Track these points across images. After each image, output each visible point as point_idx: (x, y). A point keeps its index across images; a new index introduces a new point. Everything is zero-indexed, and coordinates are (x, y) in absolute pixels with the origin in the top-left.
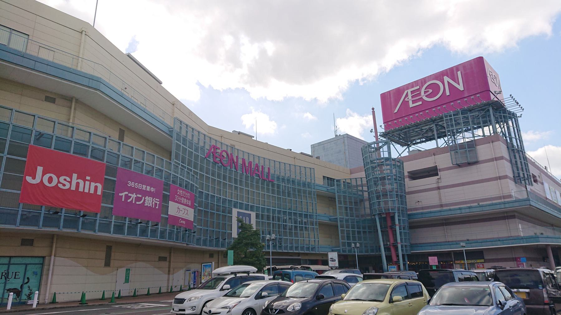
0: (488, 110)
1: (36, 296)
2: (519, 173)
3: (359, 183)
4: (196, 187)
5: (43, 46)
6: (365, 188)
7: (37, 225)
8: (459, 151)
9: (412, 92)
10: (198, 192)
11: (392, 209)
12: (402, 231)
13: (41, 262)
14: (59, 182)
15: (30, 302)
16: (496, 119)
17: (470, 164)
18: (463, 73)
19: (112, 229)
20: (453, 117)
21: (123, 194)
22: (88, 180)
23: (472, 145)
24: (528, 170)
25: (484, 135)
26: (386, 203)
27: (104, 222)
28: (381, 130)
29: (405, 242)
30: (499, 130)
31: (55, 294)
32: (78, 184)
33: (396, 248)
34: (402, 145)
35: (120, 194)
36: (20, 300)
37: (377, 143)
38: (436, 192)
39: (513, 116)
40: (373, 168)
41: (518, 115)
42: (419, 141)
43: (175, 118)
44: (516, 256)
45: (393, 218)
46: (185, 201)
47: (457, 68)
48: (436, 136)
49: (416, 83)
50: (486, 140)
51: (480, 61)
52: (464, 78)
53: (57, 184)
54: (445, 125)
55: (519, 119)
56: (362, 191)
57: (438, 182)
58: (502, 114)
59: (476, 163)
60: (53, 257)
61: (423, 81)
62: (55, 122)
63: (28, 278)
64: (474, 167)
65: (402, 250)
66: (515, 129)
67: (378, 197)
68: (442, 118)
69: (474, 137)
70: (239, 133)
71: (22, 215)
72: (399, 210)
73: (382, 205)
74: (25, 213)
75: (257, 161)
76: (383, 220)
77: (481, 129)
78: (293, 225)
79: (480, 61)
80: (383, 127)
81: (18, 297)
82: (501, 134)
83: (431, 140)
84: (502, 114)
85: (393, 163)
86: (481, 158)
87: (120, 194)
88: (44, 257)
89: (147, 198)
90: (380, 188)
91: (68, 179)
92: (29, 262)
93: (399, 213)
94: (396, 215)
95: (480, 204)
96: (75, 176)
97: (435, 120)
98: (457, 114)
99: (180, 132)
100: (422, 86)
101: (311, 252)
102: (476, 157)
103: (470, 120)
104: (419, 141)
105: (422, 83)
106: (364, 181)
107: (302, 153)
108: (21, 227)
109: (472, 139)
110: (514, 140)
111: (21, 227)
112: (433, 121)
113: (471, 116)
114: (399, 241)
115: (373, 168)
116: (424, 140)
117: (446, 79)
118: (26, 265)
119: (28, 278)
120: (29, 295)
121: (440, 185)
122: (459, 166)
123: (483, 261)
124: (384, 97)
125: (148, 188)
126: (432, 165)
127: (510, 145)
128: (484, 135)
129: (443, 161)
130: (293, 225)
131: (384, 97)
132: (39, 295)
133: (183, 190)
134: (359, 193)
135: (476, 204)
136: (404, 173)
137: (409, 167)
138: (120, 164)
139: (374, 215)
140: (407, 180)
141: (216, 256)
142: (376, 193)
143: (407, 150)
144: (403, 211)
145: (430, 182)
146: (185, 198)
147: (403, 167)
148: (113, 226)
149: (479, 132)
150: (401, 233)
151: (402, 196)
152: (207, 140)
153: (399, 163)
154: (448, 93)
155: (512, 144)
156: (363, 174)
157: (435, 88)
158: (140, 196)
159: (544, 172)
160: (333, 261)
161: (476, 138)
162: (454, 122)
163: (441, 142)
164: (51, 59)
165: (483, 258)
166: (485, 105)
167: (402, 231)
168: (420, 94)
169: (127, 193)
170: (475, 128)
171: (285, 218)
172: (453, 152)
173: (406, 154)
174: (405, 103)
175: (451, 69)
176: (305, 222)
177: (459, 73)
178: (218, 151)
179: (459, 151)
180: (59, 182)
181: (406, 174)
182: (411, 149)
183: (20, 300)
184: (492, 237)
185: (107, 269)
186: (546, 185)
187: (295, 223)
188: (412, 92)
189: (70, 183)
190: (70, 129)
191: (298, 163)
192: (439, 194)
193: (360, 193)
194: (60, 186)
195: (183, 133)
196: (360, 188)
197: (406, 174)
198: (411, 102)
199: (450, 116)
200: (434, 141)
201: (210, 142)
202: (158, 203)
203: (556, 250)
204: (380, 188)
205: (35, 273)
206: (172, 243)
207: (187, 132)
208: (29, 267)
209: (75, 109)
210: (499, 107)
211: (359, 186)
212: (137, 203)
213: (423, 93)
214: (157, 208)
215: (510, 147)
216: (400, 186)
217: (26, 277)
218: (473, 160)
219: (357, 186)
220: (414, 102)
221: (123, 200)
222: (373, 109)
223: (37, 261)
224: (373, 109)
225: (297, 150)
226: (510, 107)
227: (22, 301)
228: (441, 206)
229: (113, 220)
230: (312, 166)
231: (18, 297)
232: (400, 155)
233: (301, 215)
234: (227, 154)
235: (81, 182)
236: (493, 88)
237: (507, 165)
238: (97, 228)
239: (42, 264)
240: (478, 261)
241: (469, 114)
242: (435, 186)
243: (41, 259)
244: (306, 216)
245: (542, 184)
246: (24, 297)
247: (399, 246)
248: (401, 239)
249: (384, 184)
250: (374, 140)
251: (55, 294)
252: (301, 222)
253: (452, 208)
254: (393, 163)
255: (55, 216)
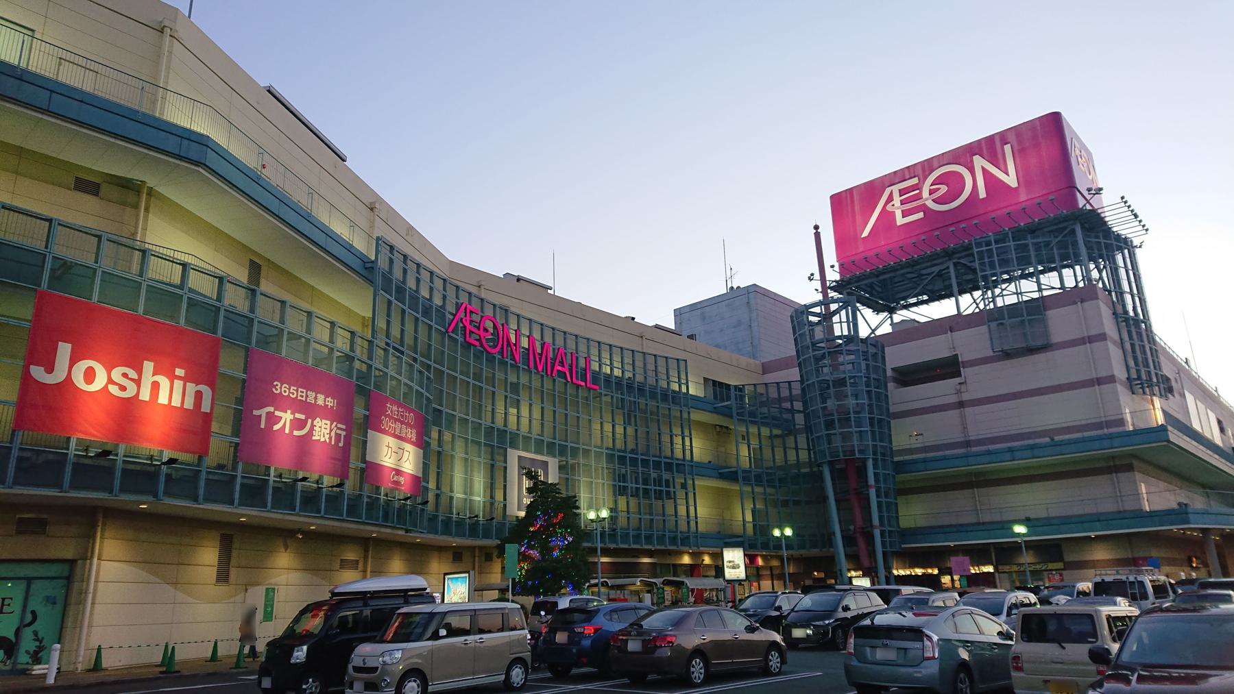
0: (1073, 232)
1: (55, 656)
2: (1138, 371)
3: (785, 393)
4: (428, 399)
5: (68, 56)
6: (798, 405)
7: (58, 485)
8: (1007, 321)
9: (902, 192)
10: (431, 411)
11: (860, 452)
12: (883, 499)
13: (66, 574)
14: (110, 381)
15: (38, 670)
16: (1089, 248)
17: (1031, 351)
18: (1016, 147)
19: (237, 495)
20: (994, 246)
21: (263, 412)
22: (179, 378)
23: (1037, 308)
24: (1157, 366)
25: (1063, 287)
26: (846, 437)
27: (216, 478)
28: (833, 275)
29: (890, 525)
30: (1095, 274)
31: (99, 649)
32: (155, 386)
33: (869, 538)
34: (877, 310)
35: (256, 412)
36: (14, 663)
37: (826, 302)
38: (955, 413)
39: (1124, 244)
40: (818, 359)
41: (1136, 242)
42: (914, 300)
43: (378, 239)
44: (1136, 555)
45: (861, 471)
46: (404, 431)
47: (1003, 137)
48: (955, 289)
49: (910, 172)
50: (1067, 297)
51: (1054, 122)
52: (1021, 174)
53: (106, 386)
54: (977, 265)
55: (1137, 251)
56: (792, 411)
57: (959, 392)
58: (1102, 241)
59: (1046, 347)
60: (95, 560)
61: (927, 166)
62: (100, 237)
63: (33, 612)
64: (1039, 358)
65: (883, 543)
66: (1131, 273)
67: (830, 425)
68: (968, 248)
69: (1040, 290)
70: (519, 279)
71: (20, 459)
72: (875, 453)
73: (837, 442)
74: (27, 454)
75: (560, 342)
76: (838, 475)
77: (1055, 274)
78: (641, 486)
79: (1054, 122)
80: (837, 268)
81: (9, 657)
82: (1100, 285)
83: (940, 298)
84: (1102, 241)
85: (862, 347)
86: (1056, 338)
87: (256, 412)
88: (72, 562)
89: (318, 422)
90: (831, 404)
91: (133, 374)
92: (35, 574)
93: (875, 460)
94: (870, 463)
95: (1056, 438)
96: (148, 366)
97: (954, 253)
98: (1003, 240)
99: (390, 272)
100: (925, 178)
101: (646, 547)
102: (1046, 333)
103: (1032, 253)
104: (914, 300)
105: (924, 171)
106: (797, 390)
107: (657, 327)
108: (18, 490)
109: (1036, 295)
110: (1128, 298)
111: (18, 490)
112: (948, 254)
113: (1035, 244)
114: (876, 521)
115: (818, 359)
116: (925, 297)
117: (979, 162)
118: (29, 580)
119: (33, 612)
120: (36, 653)
121: (966, 397)
122: (1007, 355)
123: (1060, 565)
124: (840, 203)
125: (321, 398)
126: (946, 354)
127: (1119, 309)
128: (1063, 287)
129: (971, 345)
130: (641, 486)
131: (840, 203)
132: (62, 651)
133: (400, 405)
134: (785, 416)
135: (1048, 440)
136: (885, 371)
137: (897, 357)
138: (254, 341)
139: (819, 465)
140: (891, 385)
141: (467, 556)
142: (825, 416)
143: (889, 321)
144: (885, 453)
145: (942, 390)
146: (402, 423)
147: (884, 358)
148: (238, 488)
149: (1051, 280)
150: (879, 503)
151: (882, 423)
152: (451, 292)
153: (877, 344)
154: (982, 194)
155: (1124, 306)
156: (794, 374)
157: (954, 182)
158: (303, 417)
159: (1183, 371)
160: (734, 568)
161: (1045, 293)
162: (996, 258)
163: (968, 303)
164: (88, 88)
165: (1061, 559)
166: (1066, 219)
167: (883, 499)
168: (919, 197)
169: (271, 409)
170: (1042, 272)
171: (623, 471)
172: (993, 325)
173: (886, 329)
174: (887, 216)
175: (990, 140)
176: (667, 481)
177: (1007, 148)
178: (474, 317)
179: (1007, 321)
180: (110, 381)
181: (889, 373)
182: (897, 318)
183: (14, 663)
184: (1081, 512)
185: (223, 589)
186: (1190, 398)
187: (646, 482)
188: (902, 192)
189: (138, 382)
190: (137, 254)
191: (650, 348)
192: (963, 417)
193: (787, 416)
194: (113, 390)
195: (397, 274)
196: (788, 405)
197: (889, 373)
198: (898, 214)
199: (988, 244)
200: (953, 299)
201: (457, 297)
202: (343, 433)
203: (1233, 540)
204: (831, 404)
205: (51, 601)
206: (388, 531)
207: (405, 271)
208: (36, 586)
209: (147, 210)
210: (1094, 223)
211: (785, 399)
212: (296, 433)
213: (925, 194)
214: (341, 445)
215: (1120, 315)
216: (878, 399)
217: (30, 608)
218: (1039, 343)
219: (780, 400)
220: (905, 214)
221: (263, 426)
222: (816, 227)
223: (53, 570)
224: (816, 227)
225: (647, 318)
226: (1118, 222)
227: (20, 667)
228: (967, 444)
229: (239, 474)
230: (681, 355)
231: (9, 657)
232: (873, 331)
233: (645, 463)
234: (495, 327)
235: (164, 381)
236: (1082, 185)
237: (1115, 353)
238: (201, 492)
239: (69, 579)
240: (1051, 566)
241: (1030, 241)
242: (953, 399)
243: (66, 567)
244: (657, 465)
245: (1183, 396)
246: (23, 658)
247: (877, 533)
248: (881, 518)
249: (840, 396)
250: (820, 297)
251: (99, 649)
252: (658, 482)
253: (991, 447)
254: (862, 347)
255: (102, 462)
